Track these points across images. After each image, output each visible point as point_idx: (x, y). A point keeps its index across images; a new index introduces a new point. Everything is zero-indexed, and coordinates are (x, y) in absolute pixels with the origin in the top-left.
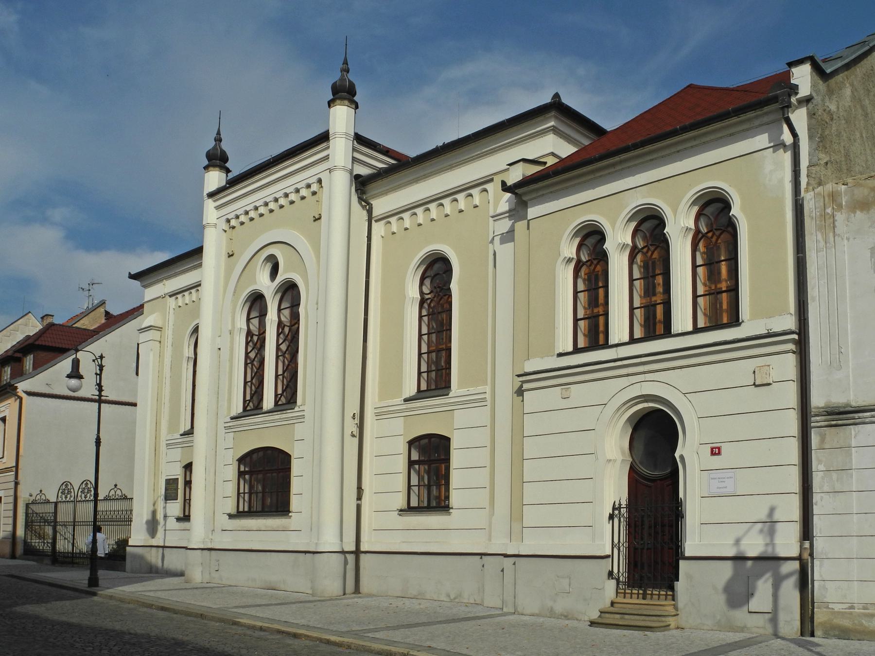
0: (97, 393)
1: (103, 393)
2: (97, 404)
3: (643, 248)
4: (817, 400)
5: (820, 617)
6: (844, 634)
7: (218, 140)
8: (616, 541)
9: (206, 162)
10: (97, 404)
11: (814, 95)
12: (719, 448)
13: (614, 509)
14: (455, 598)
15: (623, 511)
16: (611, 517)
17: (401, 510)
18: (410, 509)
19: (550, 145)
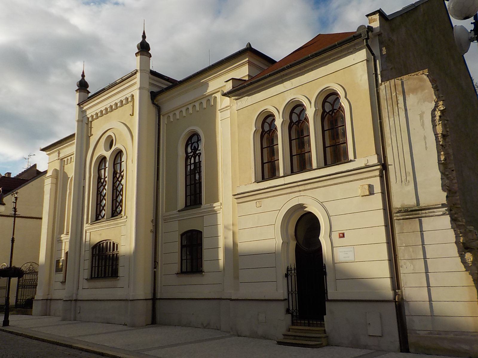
0: (14, 213)
1: (17, 213)
2: (13, 218)
3: (296, 122)
4: (397, 203)
5: (411, 339)
6: (427, 351)
7: (144, 37)
8: (290, 290)
9: (137, 51)
10: (13, 218)
11: (382, 31)
12: (343, 234)
13: (288, 270)
14: (206, 326)
15: (293, 272)
16: (287, 276)
17: (177, 274)
18: (182, 272)
19: (242, 72)
